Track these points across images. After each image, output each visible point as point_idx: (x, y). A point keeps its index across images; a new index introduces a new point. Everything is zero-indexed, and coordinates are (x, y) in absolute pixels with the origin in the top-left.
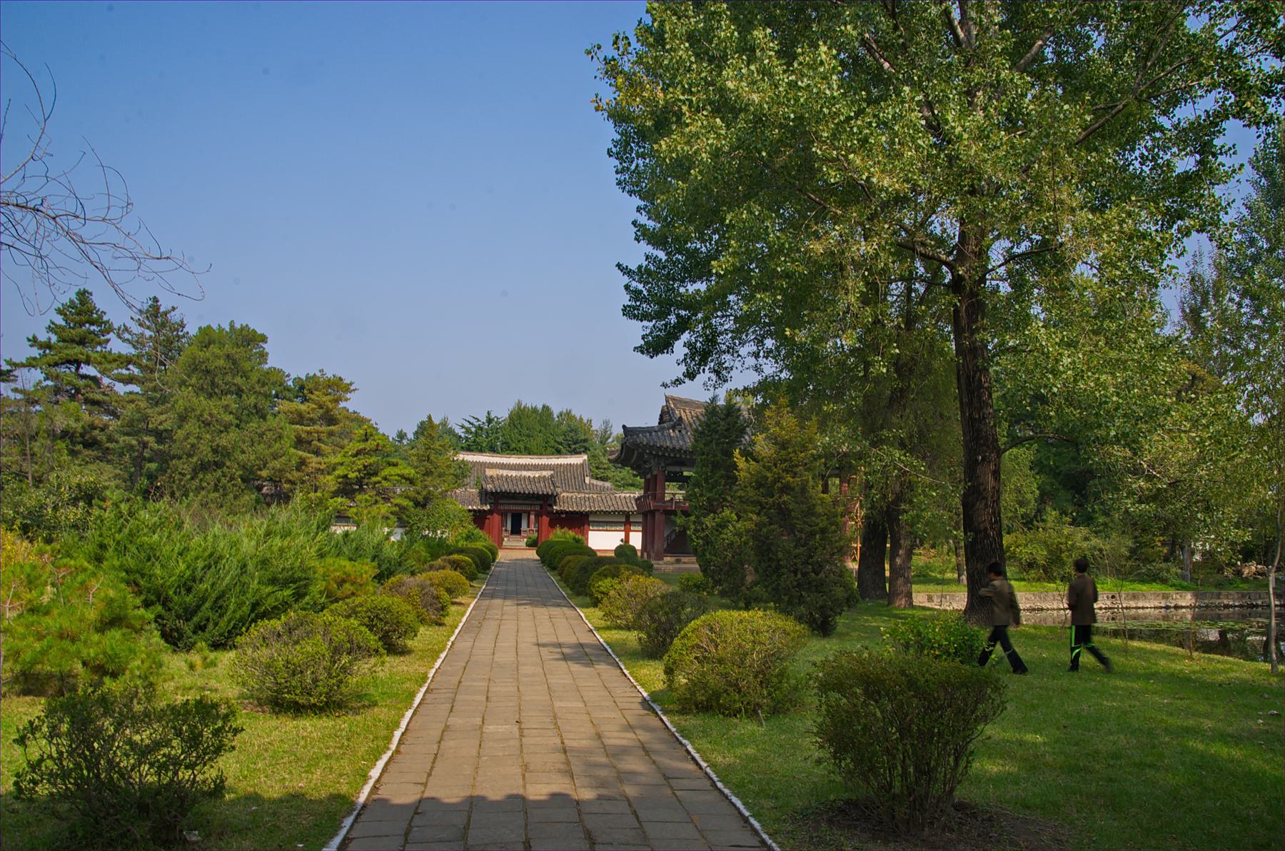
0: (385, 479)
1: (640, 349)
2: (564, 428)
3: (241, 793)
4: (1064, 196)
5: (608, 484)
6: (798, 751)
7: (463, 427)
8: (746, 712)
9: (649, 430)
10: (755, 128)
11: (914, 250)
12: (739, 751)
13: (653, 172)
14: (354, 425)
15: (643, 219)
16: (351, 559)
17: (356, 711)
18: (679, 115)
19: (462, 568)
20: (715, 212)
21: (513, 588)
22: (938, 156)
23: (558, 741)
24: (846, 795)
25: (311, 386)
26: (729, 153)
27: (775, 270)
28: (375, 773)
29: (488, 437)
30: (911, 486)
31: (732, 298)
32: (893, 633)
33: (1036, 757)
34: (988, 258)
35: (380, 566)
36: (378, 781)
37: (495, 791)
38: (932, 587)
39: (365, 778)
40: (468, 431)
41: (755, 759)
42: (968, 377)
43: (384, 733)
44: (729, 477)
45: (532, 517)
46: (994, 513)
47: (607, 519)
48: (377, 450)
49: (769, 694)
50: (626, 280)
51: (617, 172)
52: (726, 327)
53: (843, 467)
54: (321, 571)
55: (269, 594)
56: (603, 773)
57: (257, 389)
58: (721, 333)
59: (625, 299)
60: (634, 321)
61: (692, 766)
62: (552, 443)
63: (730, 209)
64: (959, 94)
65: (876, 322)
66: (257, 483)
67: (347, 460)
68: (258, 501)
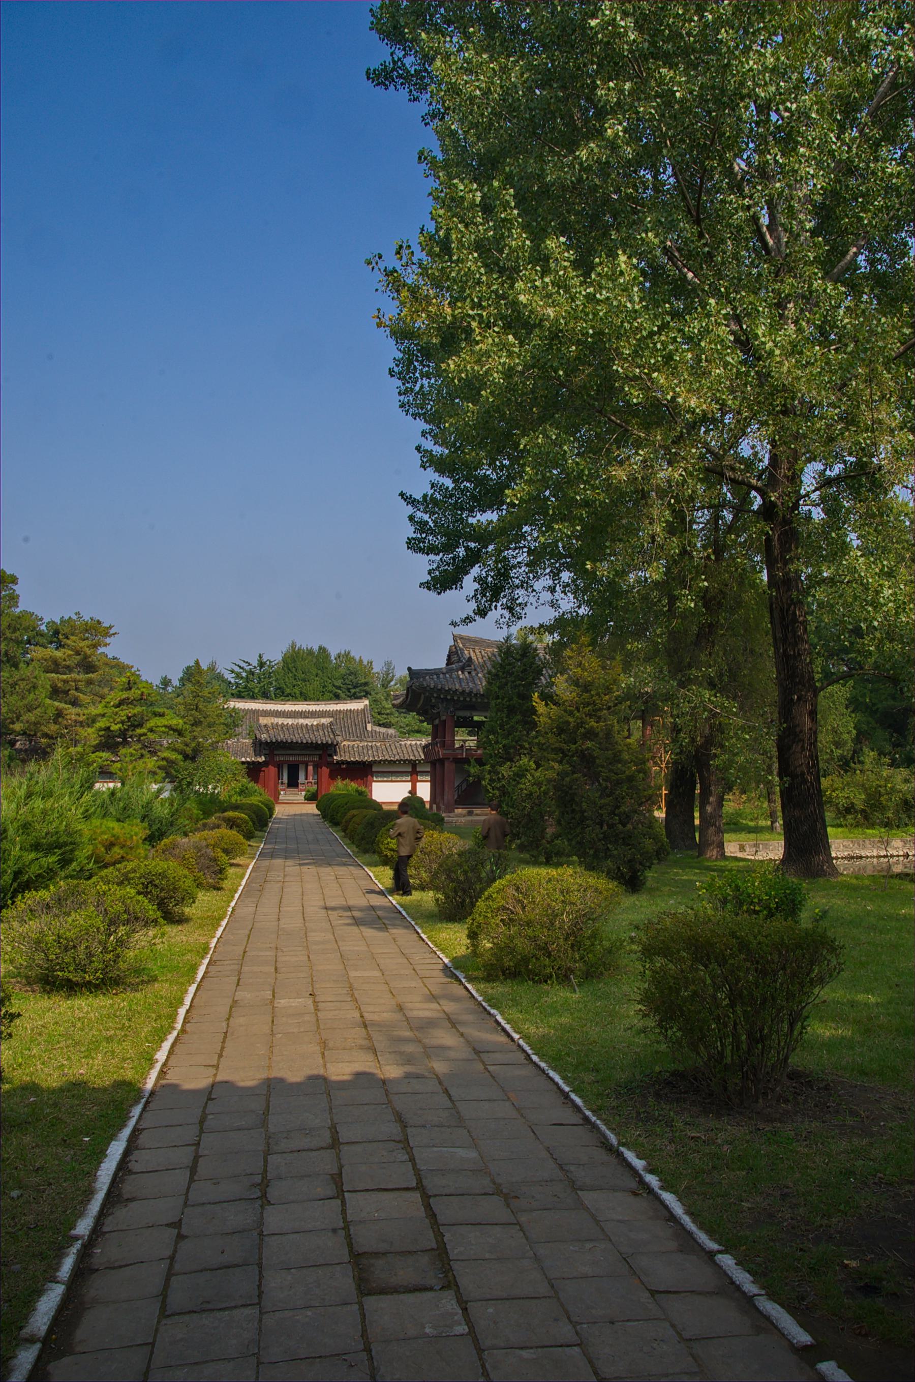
0: (151, 730)
1: (426, 585)
2: (342, 671)
3: (17, 1082)
4: (883, 416)
5: (391, 731)
6: (621, 1017)
7: (232, 671)
8: (557, 978)
9: (436, 672)
10: (551, 345)
11: (722, 475)
12: (553, 1020)
13: (439, 392)
14: (114, 672)
15: (429, 444)
16: (119, 820)
17: (135, 988)
18: (469, 331)
19: (238, 826)
20: (508, 435)
21: (294, 846)
22: (747, 374)
23: (357, 1014)
24: (673, 1067)
25: (66, 630)
26: (522, 373)
27: (574, 499)
28: (161, 1056)
29: (262, 682)
30: (721, 729)
31: (526, 528)
32: (710, 887)
33: (870, 1018)
34: (801, 482)
35: (150, 826)
36: (165, 1064)
37: (294, 1069)
38: (743, 836)
39: (151, 1062)
40: (238, 676)
41: (570, 1029)
42: (782, 611)
43: (166, 1011)
44: (526, 723)
45: (310, 768)
46: (811, 756)
47: (392, 769)
48: (141, 699)
49: (582, 958)
50: (410, 510)
51: (400, 394)
52: (519, 560)
53: (646, 708)
54: (87, 834)
55: (33, 861)
56: (410, 1048)
57: (9, 635)
58: (514, 567)
59: (410, 531)
60: (420, 555)
61: (503, 1039)
62: (330, 688)
63: (524, 434)
64: (770, 307)
65: (684, 552)
66: (9, 737)
67: (109, 711)
68: (11, 758)
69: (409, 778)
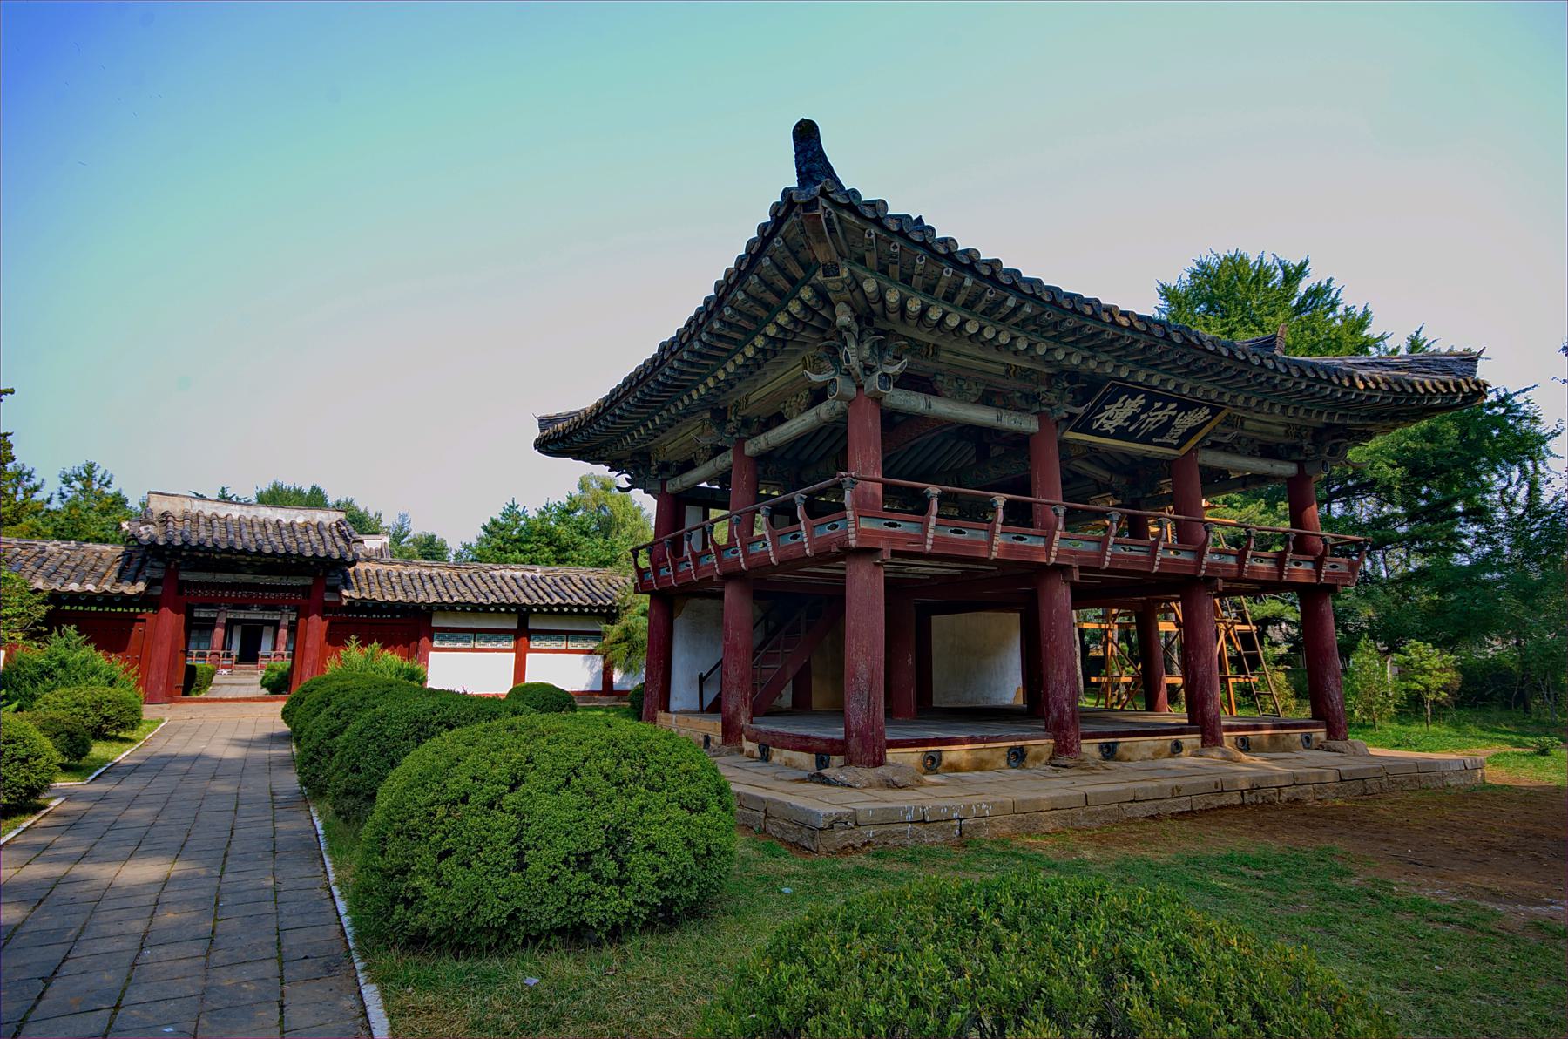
45: (283, 633)
69: (511, 645)
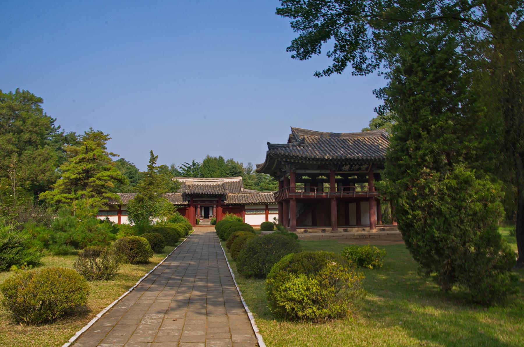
2: (230, 166)
7: (181, 168)
29: (193, 171)
40: (184, 170)
45: (215, 209)
